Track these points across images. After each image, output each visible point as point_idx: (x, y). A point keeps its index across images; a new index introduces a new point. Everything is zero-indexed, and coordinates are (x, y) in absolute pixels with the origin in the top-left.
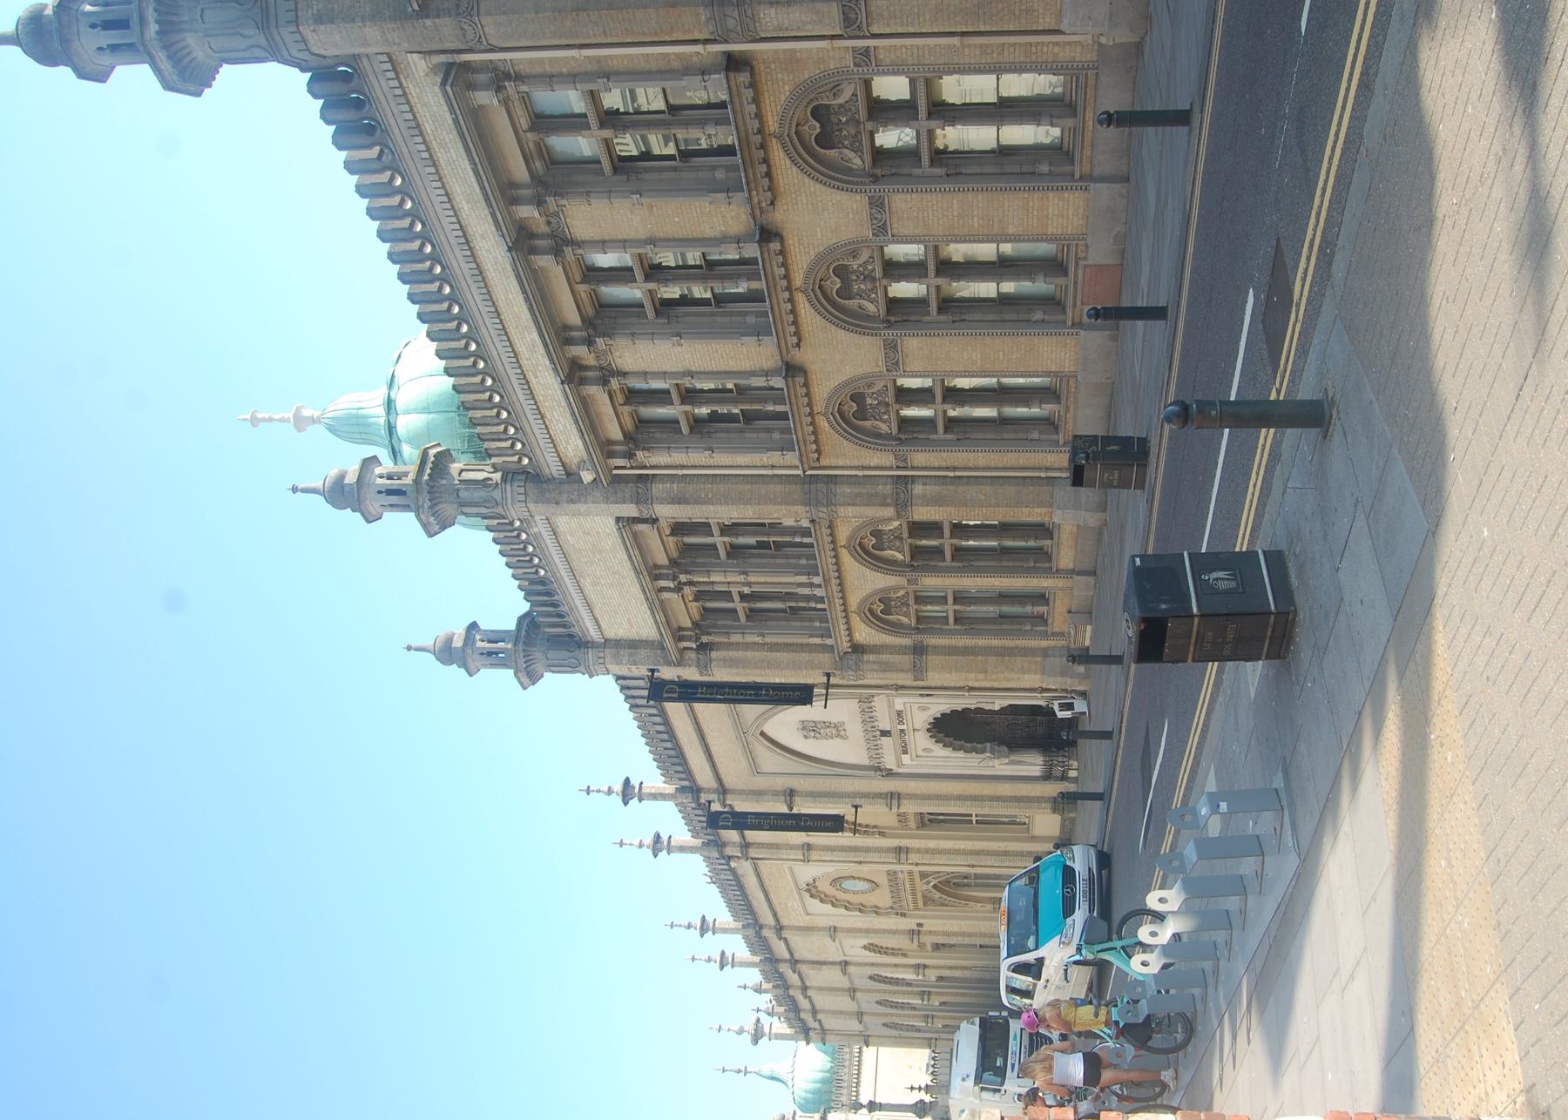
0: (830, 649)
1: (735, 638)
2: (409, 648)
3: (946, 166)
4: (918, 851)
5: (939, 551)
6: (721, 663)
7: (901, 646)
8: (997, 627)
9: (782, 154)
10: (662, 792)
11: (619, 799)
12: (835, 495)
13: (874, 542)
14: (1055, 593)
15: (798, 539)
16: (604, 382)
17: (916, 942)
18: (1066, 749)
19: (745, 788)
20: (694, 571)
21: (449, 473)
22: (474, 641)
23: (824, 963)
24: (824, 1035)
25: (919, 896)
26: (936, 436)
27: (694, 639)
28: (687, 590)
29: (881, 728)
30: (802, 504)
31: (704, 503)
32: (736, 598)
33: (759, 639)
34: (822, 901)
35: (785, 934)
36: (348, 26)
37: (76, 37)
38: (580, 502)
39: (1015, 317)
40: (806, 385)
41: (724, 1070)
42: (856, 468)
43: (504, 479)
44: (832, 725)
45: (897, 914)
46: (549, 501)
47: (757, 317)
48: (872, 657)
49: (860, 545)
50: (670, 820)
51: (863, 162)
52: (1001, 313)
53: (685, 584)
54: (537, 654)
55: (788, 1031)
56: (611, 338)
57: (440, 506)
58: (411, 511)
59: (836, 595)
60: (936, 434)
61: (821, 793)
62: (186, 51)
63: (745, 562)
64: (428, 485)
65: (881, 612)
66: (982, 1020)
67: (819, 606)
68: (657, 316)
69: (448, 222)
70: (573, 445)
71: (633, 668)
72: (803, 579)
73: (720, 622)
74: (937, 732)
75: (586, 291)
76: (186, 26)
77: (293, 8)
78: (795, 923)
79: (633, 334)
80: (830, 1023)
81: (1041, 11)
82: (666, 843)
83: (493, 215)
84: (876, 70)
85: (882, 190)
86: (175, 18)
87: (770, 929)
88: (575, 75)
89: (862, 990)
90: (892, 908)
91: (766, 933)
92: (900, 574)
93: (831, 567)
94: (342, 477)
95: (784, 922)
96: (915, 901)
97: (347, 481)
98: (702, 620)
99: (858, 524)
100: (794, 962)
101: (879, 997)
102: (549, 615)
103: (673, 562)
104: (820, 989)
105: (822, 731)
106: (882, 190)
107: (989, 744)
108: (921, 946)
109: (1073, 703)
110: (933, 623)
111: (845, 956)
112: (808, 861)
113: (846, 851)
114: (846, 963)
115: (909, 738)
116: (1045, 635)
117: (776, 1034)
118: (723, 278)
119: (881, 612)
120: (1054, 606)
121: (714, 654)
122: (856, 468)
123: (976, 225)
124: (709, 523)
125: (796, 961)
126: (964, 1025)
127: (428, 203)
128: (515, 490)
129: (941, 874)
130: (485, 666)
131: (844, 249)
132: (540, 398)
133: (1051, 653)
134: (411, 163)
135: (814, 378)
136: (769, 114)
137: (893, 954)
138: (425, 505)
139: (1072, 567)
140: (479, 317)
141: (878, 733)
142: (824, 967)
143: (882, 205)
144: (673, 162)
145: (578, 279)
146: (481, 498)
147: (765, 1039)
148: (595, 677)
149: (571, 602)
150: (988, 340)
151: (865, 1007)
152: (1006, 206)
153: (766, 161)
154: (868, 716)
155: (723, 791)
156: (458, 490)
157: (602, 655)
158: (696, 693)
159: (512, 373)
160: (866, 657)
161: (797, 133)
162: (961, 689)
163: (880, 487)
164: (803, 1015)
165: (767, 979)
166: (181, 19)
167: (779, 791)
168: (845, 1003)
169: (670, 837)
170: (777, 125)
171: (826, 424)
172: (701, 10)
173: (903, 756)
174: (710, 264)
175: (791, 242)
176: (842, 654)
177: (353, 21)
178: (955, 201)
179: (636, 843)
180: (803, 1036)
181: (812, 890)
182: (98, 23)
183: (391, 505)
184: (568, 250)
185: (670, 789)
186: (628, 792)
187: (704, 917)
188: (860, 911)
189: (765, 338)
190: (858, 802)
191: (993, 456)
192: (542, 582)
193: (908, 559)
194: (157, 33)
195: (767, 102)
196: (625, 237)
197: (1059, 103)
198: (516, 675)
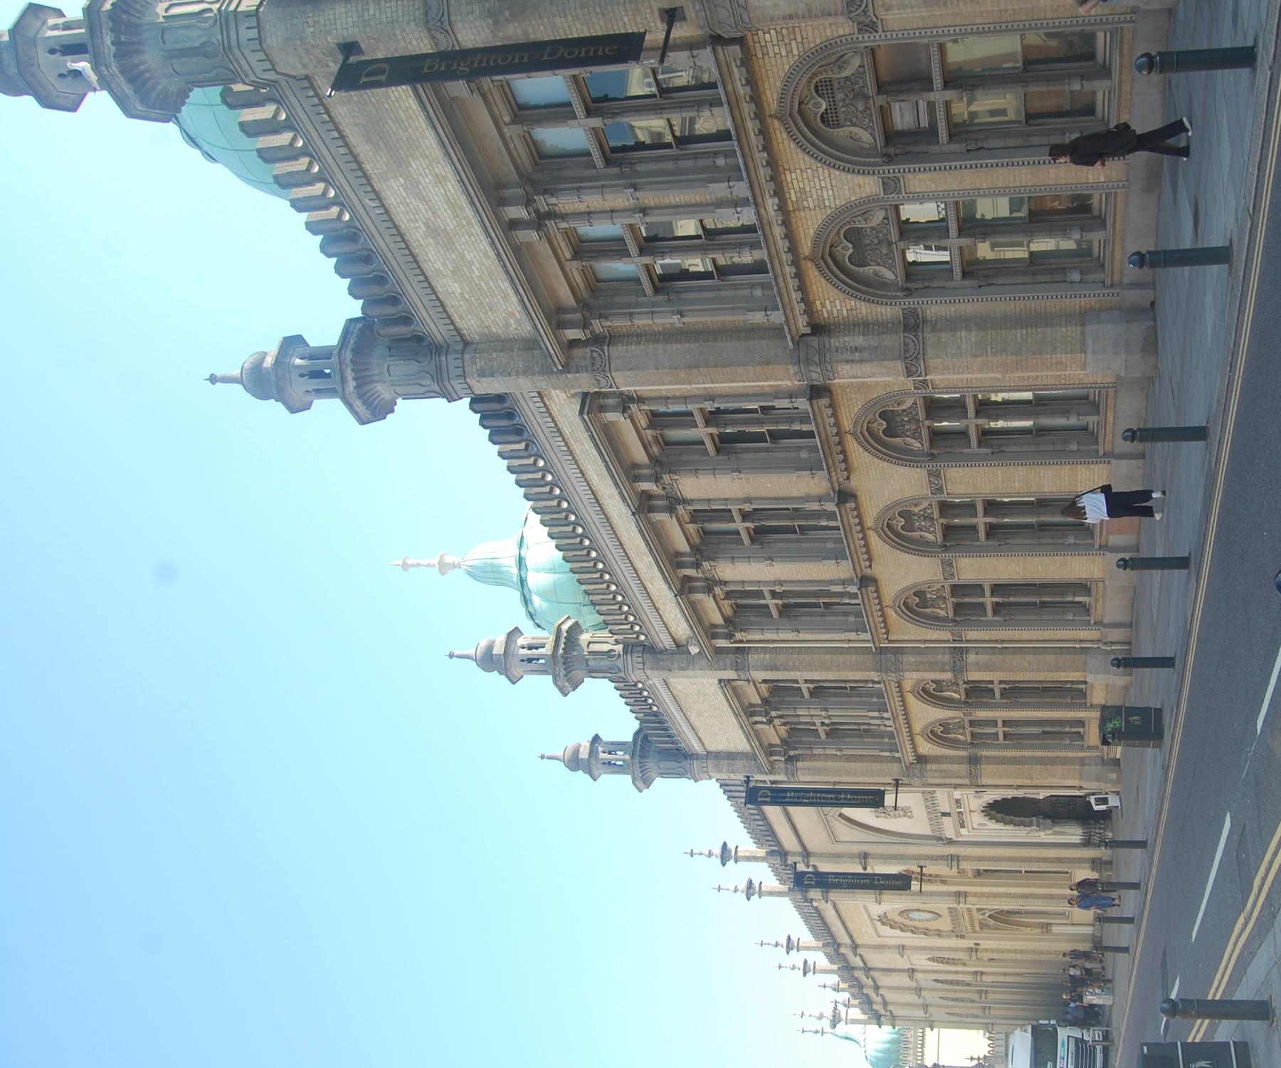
0: (898, 760)
1: (642, 322)
2: (213, 379)
3: (992, 447)
4: (975, 895)
5: (962, 434)
6: (806, 771)
7: (959, 757)
8: (1041, 742)
9: (856, 444)
10: (755, 855)
11: (719, 861)
12: (902, 663)
15: (796, 427)
16: (671, 510)
17: (955, 868)
18: (1102, 822)
19: (825, 851)
21: (579, 645)
22: (597, 753)
24: (893, 1020)
25: (977, 923)
26: (953, 283)
27: (782, 753)
28: (777, 722)
29: (942, 811)
30: (874, 671)
31: (792, 670)
32: (767, 595)
34: (891, 927)
35: (860, 951)
36: (507, 378)
37: (289, 385)
39: (1051, 541)
40: (877, 591)
41: (803, 1031)
42: (920, 641)
43: (625, 651)
45: (957, 936)
46: (663, 669)
47: (835, 543)
48: (934, 766)
49: (889, 526)
50: (764, 874)
51: (923, 445)
52: (1039, 538)
53: (775, 717)
54: (651, 764)
55: (863, 1017)
56: (714, 561)
57: (573, 673)
59: (900, 713)
60: (970, 448)
61: (891, 855)
62: (376, 395)
63: (737, 458)
64: (563, 657)
65: (940, 734)
66: (1033, 1027)
67: (853, 601)
68: (656, 293)
69: (582, 489)
70: (682, 629)
72: (876, 714)
73: (804, 739)
75: (577, 269)
76: (376, 378)
77: (255, 25)
78: (867, 942)
79: (733, 558)
80: (898, 1011)
81: (1068, 363)
82: (757, 889)
83: (621, 494)
84: (883, 37)
85: (897, 171)
86: (367, 373)
87: (846, 947)
88: (686, 398)
89: (927, 989)
90: (953, 931)
91: (857, 974)
92: (957, 709)
93: (898, 708)
94: (490, 647)
95: (859, 941)
96: (973, 927)
97: (265, 365)
98: (789, 737)
100: (867, 969)
101: (942, 994)
102: (660, 735)
103: (765, 701)
104: (890, 988)
106: (897, 171)
107: (1035, 818)
108: (961, 872)
109: (1107, 798)
110: (985, 739)
114: (913, 970)
116: (1082, 748)
117: (851, 1020)
118: (723, 248)
119: (883, 432)
121: (800, 764)
122: (920, 641)
123: (1017, 487)
125: (870, 969)
126: (1018, 1032)
127: (566, 478)
128: (634, 659)
130: (526, 672)
131: (859, 209)
132: (655, 598)
133: (1086, 762)
134: (552, 454)
135: (863, 498)
136: (845, 419)
137: (954, 964)
138: (561, 674)
140: (606, 549)
142: (893, 974)
143: (951, 565)
146: (607, 666)
150: (1028, 559)
152: (1042, 475)
153: (843, 452)
154: (930, 803)
155: (806, 854)
156: (587, 660)
157: (705, 765)
158: (786, 797)
159: (634, 584)
160: (929, 766)
161: (800, 111)
163: (940, 657)
165: (843, 979)
166: (372, 373)
167: (854, 854)
169: (761, 883)
170: (851, 426)
171: (893, 613)
172: (790, 367)
174: (710, 233)
175: (863, 498)
177: (510, 375)
178: (999, 472)
179: (732, 888)
180: (875, 1021)
181: (884, 920)
182: (57, 48)
184: (634, 407)
185: (785, 888)
186: (726, 854)
187: (789, 936)
188: (925, 934)
189: (843, 561)
190: (922, 863)
191: (1037, 633)
192: (655, 714)
193: (963, 697)
194: (355, 388)
195: (843, 412)
196: (727, 497)
197: (1084, 401)
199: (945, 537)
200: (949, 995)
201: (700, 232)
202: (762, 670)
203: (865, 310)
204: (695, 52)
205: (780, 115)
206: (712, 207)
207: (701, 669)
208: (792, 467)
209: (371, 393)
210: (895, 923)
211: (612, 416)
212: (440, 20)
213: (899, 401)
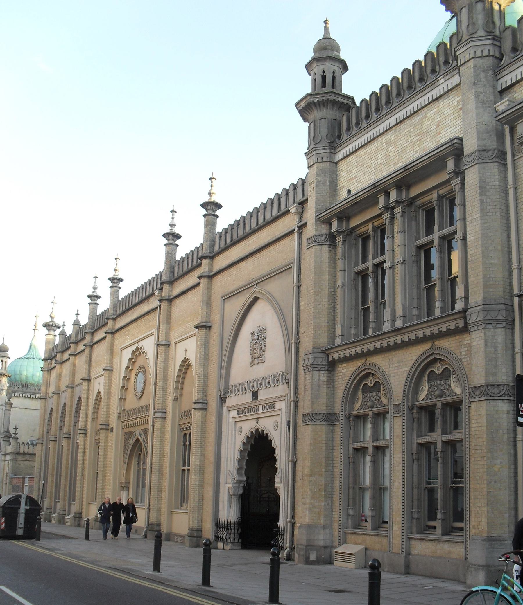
1: (340, 264)
11: (112, 276)
13: (370, 385)
14: (387, 536)
18: (240, 541)
20: (404, 222)
23: (90, 365)
25: (132, 429)
26: (351, 443)
32: (447, 230)
33: (339, 283)
34: (130, 359)
35: (109, 337)
38: (477, 103)
44: (263, 353)
58: (312, 92)
71: (314, 185)
74: (255, 437)
87: (112, 325)
89: (73, 392)
95: (117, 335)
96: (128, 426)
99: (458, 355)
101: (84, 397)
105: (257, 345)
108: (188, 414)
111: (176, 343)
112: (157, 345)
113: (164, 372)
114: (89, 380)
115: (251, 415)
120: (372, 535)
124: (432, 233)
129: (146, 444)
137: (94, 413)
139: (412, 552)
141: (256, 389)
142: (87, 365)
144: (447, 276)
145: (441, 192)
147: (46, 332)
148: (305, 158)
149: (371, 128)
151: (63, 395)
157: (324, 160)
162: (295, 454)
164: (205, 263)
168: (65, 382)
173: (236, 411)
174: (453, 281)
176: (327, 352)
181: (138, 353)
183: (315, 80)
186: (116, 281)
188: (123, 387)
193: (420, 403)
198: (308, 95)
199: (421, 408)
200: (68, 409)
201: (453, 276)
202: (480, 177)
203: (340, 393)
204: (463, 299)
205: (433, 347)
206: (392, 307)
207: (477, 114)
208: (344, 322)
209: (310, 112)
210: (134, 362)
211: (450, 165)
212: (479, 158)
213: (387, 395)
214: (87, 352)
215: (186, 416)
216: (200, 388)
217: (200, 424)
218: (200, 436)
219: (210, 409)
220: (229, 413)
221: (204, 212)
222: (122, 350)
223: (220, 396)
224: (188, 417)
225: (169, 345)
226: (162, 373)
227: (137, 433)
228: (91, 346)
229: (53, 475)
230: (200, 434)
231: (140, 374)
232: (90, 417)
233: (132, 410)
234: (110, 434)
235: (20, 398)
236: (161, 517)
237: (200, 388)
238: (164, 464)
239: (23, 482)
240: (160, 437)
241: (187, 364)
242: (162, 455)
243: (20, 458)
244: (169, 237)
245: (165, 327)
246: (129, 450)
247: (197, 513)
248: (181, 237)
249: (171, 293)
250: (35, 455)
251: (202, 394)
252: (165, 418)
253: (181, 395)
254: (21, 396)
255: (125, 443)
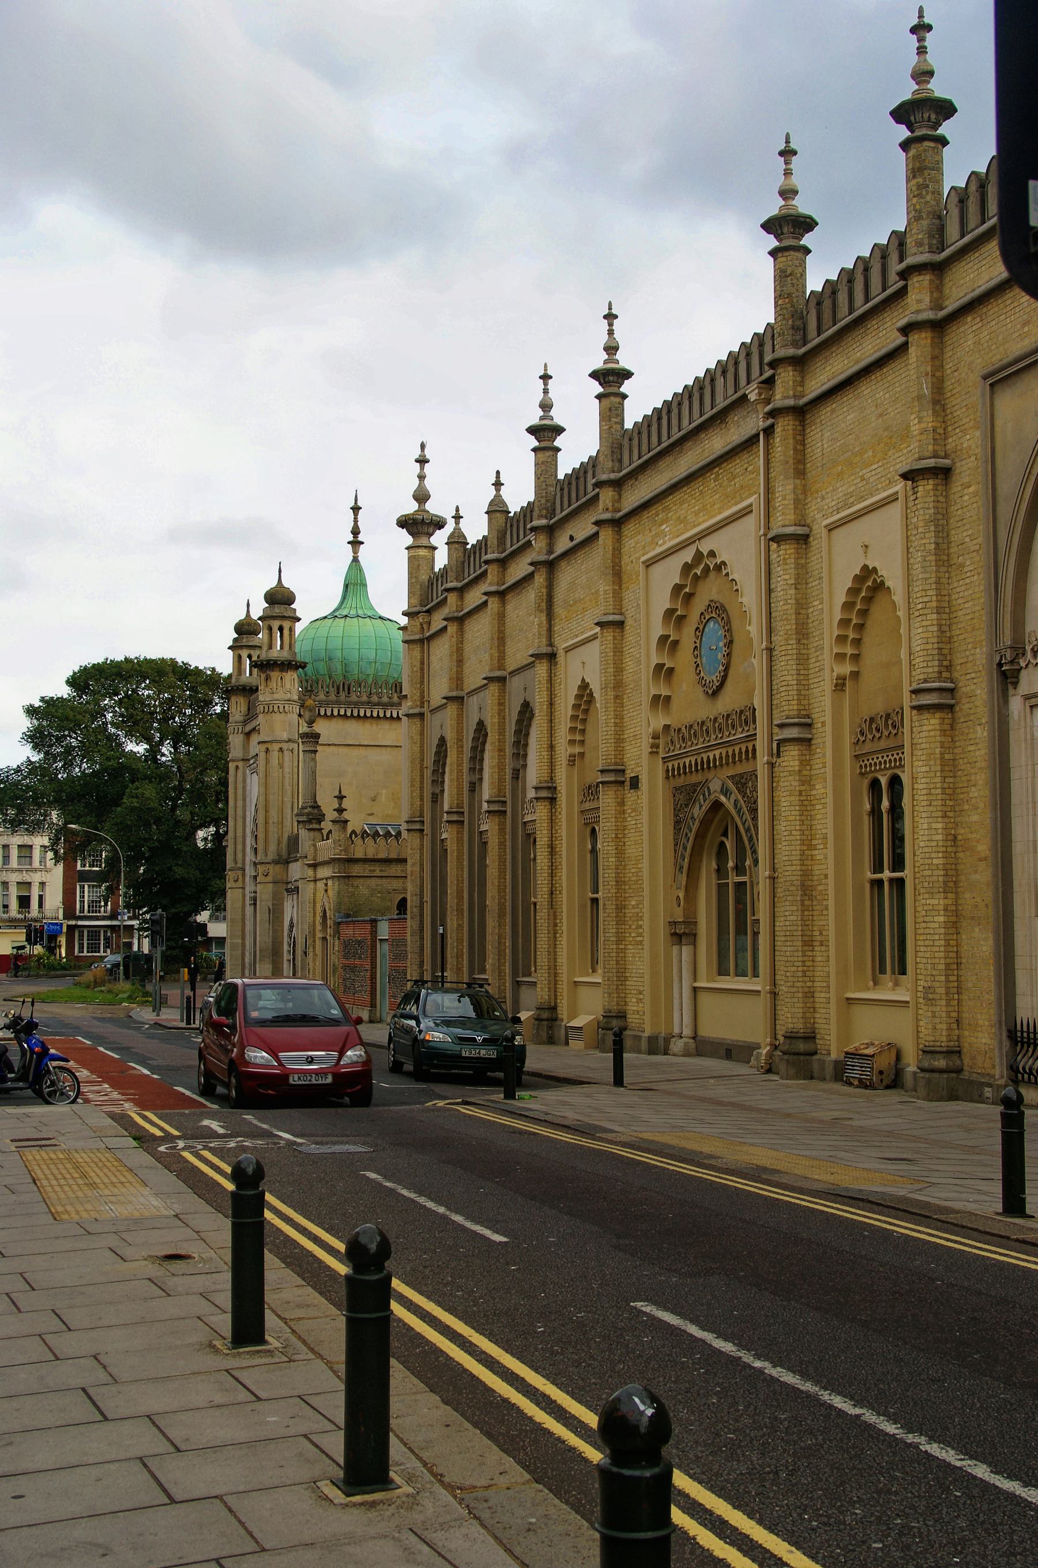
25: (695, 778)
34: (677, 589)
96: (684, 771)
113: (798, 614)
142: (543, 617)
210: (689, 597)
214: (540, 579)
215: (878, 730)
216: (930, 646)
217: (938, 751)
218: (939, 785)
219: (964, 707)
220: (1032, 713)
221: (903, 132)
222: (649, 564)
223: (1000, 665)
224: (870, 737)
225: (807, 536)
226: (794, 617)
227: (715, 785)
228: (551, 566)
229: (460, 911)
230: (938, 780)
231: (711, 624)
232: (563, 751)
233: (680, 730)
234: (630, 796)
235: (334, 721)
236: (817, 1015)
237: (930, 646)
238: (815, 867)
239: (374, 933)
240: (800, 794)
241: (870, 583)
242: (808, 843)
243: (357, 869)
244: (781, 227)
245: (791, 487)
246: (692, 836)
247: (944, 1003)
248: (817, 224)
249: (799, 389)
250: (405, 861)
251: (936, 663)
252: (810, 740)
253: (855, 675)
254: (336, 713)
255: (676, 815)
